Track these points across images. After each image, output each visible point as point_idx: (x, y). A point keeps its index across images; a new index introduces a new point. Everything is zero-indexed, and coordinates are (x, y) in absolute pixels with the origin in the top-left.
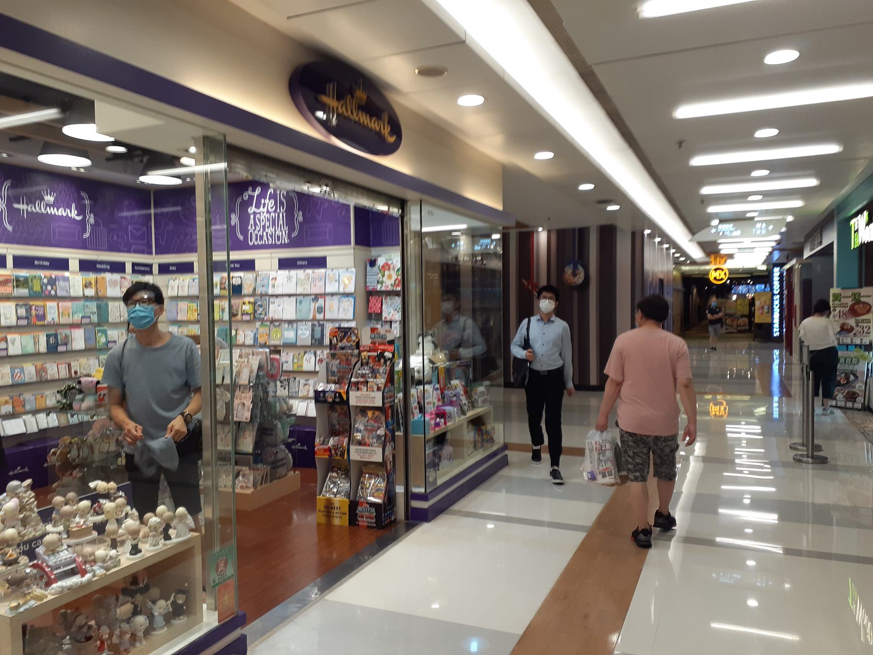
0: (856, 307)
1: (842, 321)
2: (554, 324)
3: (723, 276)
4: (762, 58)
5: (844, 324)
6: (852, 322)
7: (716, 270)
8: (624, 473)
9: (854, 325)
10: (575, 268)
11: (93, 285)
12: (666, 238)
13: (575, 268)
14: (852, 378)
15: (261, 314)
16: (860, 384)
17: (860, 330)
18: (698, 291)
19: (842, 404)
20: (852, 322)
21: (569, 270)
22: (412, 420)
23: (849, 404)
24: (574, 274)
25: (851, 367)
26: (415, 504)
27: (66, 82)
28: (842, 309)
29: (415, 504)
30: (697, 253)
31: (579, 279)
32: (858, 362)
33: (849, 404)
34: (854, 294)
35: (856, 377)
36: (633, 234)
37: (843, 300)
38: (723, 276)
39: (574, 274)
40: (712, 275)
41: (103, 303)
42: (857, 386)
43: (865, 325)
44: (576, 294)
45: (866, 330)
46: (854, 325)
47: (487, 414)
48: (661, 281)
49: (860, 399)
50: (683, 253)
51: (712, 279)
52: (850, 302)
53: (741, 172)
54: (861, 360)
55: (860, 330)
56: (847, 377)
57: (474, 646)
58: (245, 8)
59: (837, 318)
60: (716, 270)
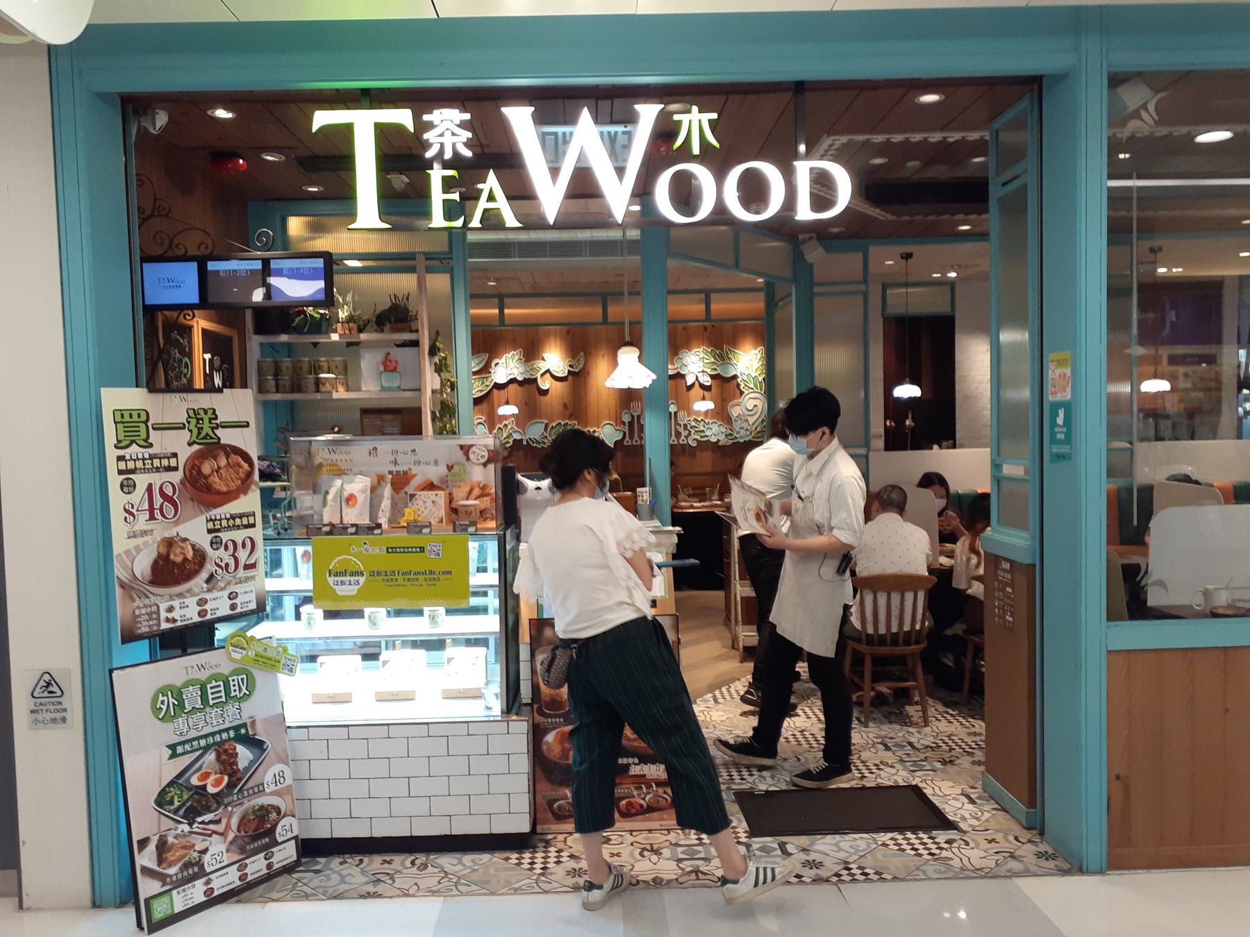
0: (206, 468)
1: (162, 530)
2: (1167, 475)
5: (169, 543)
6: (195, 530)
9: (204, 541)
11: (73, 701)
14: (244, 755)
16: (277, 768)
17: (227, 558)
19: (230, 879)
20: (195, 530)
22: (1027, 462)
23: (257, 866)
25: (232, 716)
28: (157, 479)
32: (251, 684)
33: (257, 866)
34: (195, 415)
35: (256, 744)
37: (162, 442)
41: (210, 386)
42: (269, 778)
43: (239, 535)
45: (243, 555)
46: (204, 541)
49: (287, 828)
52: (180, 445)
54: (259, 676)
55: (227, 558)
56: (227, 762)
57: (947, 915)
58: (899, 7)
59: (142, 521)
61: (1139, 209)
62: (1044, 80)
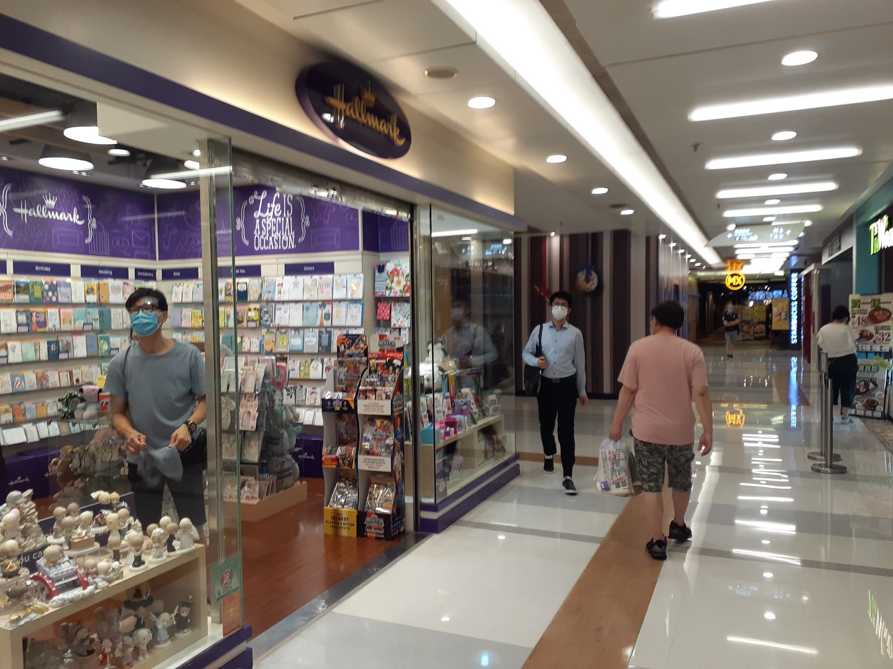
0: (876, 314)
1: (861, 328)
2: (567, 331)
3: (739, 282)
4: (780, 59)
5: (863, 331)
6: (871, 329)
7: (732, 276)
8: (638, 483)
9: (874, 332)
10: (588, 274)
12: (681, 243)
13: (588, 274)
14: (871, 386)
15: (267, 321)
16: (880, 392)
17: (880, 337)
18: (714, 297)
19: (861, 412)
20: (871, 329)
21: (582, 276)
22: (421, 429)
23: (869, 413)
24: (588, 280)
25: (870, 375)
26: (425, 515)
27: (68, 84)
28: (861, 316)
29: (425, 515)
30: (713, 259)
31: (593, 285)
32: (878, 370)
33: (869, 413)
34: (874, 301)
35: (876, 385)
36: (648, 239)
37: (863, 307)
38: (739, 282)
39: (588, 280)
40: (729, 281)
42: (877, 394)
43: (885, 332)
44: (589, 301)
45: (885, 337)
46: (874, 332)
47: (499, 422)
48: (676, 287)
49: (880, 408)
50: (699, 259)
51: (728, 285)
52: (869, 308)
53: (758, 175)
54: (880, 368)
55: (880, 337)
56: (866, 385)
57: (485, 660)
58: (251, 8)
59: (856, 325)
60: (732, 276)
61: (154, 220)
62: (320, 479)
